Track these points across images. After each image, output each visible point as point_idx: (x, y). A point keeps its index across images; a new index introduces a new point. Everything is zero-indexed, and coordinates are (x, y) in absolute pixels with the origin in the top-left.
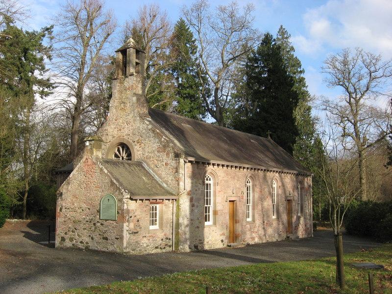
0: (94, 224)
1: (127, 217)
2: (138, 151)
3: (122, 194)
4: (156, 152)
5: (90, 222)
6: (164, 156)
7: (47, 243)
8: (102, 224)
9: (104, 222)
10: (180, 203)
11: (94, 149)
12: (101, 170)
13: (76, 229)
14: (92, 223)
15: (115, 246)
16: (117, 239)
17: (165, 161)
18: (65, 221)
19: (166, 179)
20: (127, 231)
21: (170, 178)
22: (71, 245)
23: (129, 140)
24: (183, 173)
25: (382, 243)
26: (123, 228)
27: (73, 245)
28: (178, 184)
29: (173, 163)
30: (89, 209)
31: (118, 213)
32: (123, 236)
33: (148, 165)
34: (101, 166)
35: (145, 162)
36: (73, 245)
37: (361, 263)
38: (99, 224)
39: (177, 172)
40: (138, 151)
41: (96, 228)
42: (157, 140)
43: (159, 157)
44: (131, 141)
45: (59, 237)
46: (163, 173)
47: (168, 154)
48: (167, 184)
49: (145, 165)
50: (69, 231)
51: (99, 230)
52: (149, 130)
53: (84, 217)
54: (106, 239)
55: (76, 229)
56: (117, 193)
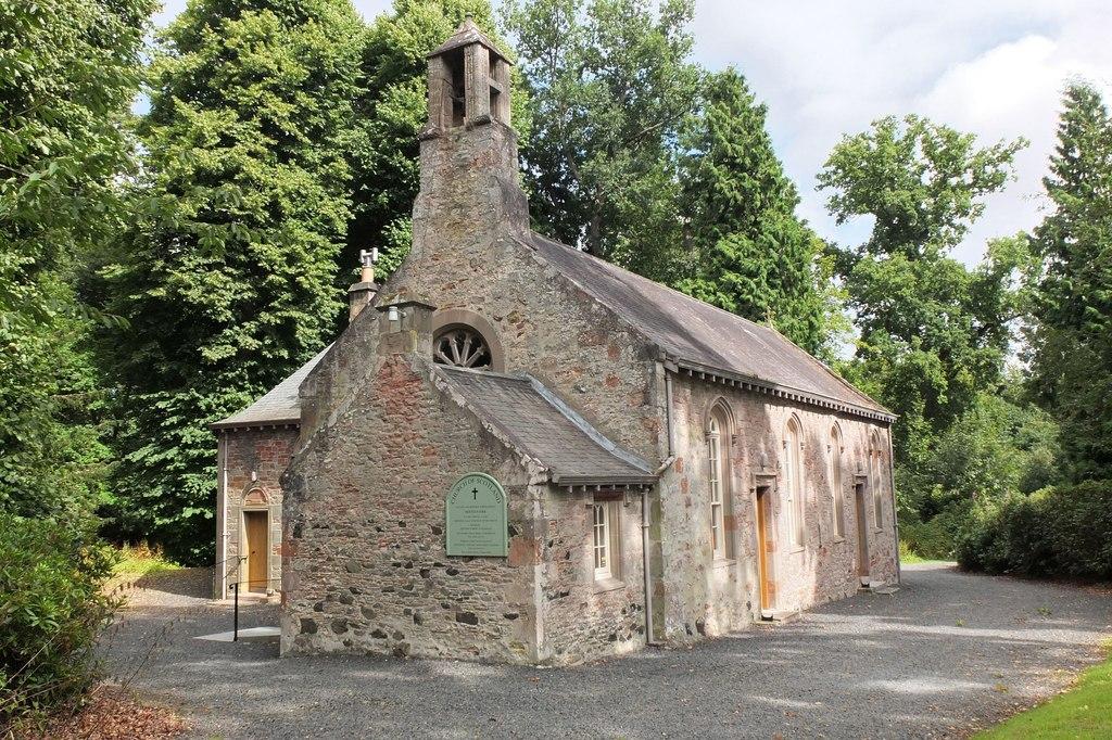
0: (423, 573)
1: (543, 547)
2: (513, 345)
3: (524, 469)
4: (575, 347)
5: (409, 566)
6: (600, 358)
7: (228, 636)
8: (453, 573)
9: (462, 566)
10: (663, 494)
11: (413, 333)
12: (444, 396)
13: (354, 591)
14: (416, 569)
15: (505, 641)
16: (512, 617)
17: (606, 372)
18: (315, 569)
19: (611, 425)
20: (545, 589)
21: (624, 424)
22: (340, 645)
23: (484, 316)
24: (664, 404)
25: (816, 592)
26: (532, 580)
27: (347, 644)
28: (656, 440)
29: (635, 378)
30: (402, 524)
31: (512, 532)
32: (534, 608)
33: (549, 386)
34: (441, 386)
35: (539, 378)
36: (347, 644)
37: (1061, 646)
38: (441, 572)
39: (647, 402)
40: (513, 345)
41: (430, 585)
42: (576, 309)
43: (584, 360)
44: (490, 319)
45: (294, 622)
46: (601, 409)
47: (614, 351)
48: (615, 440)
49: (538, 386)
50: (329, 598)
51: (443, 591)
52: (549, 281)
53: (384, 550)
54: (470, 619)
55: (354, 591)
56: (505, 468)
